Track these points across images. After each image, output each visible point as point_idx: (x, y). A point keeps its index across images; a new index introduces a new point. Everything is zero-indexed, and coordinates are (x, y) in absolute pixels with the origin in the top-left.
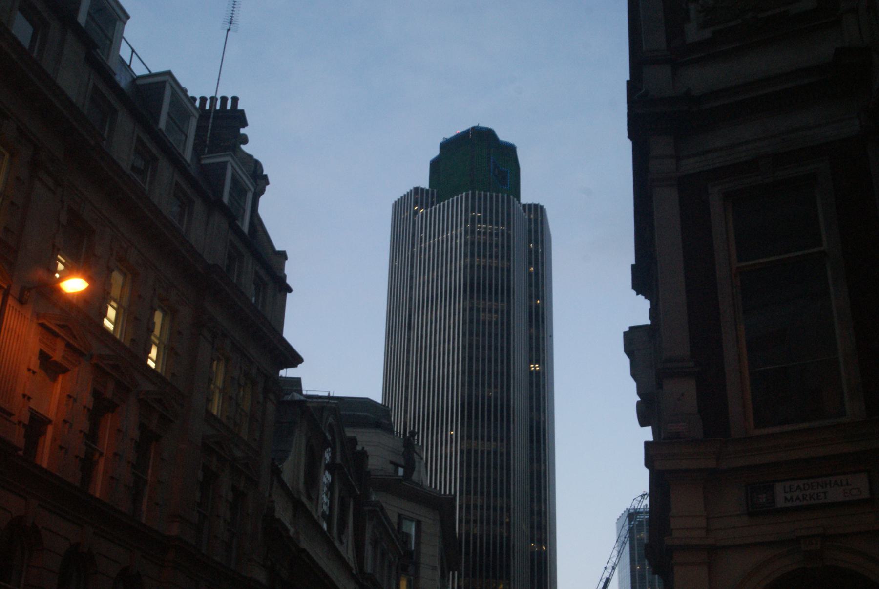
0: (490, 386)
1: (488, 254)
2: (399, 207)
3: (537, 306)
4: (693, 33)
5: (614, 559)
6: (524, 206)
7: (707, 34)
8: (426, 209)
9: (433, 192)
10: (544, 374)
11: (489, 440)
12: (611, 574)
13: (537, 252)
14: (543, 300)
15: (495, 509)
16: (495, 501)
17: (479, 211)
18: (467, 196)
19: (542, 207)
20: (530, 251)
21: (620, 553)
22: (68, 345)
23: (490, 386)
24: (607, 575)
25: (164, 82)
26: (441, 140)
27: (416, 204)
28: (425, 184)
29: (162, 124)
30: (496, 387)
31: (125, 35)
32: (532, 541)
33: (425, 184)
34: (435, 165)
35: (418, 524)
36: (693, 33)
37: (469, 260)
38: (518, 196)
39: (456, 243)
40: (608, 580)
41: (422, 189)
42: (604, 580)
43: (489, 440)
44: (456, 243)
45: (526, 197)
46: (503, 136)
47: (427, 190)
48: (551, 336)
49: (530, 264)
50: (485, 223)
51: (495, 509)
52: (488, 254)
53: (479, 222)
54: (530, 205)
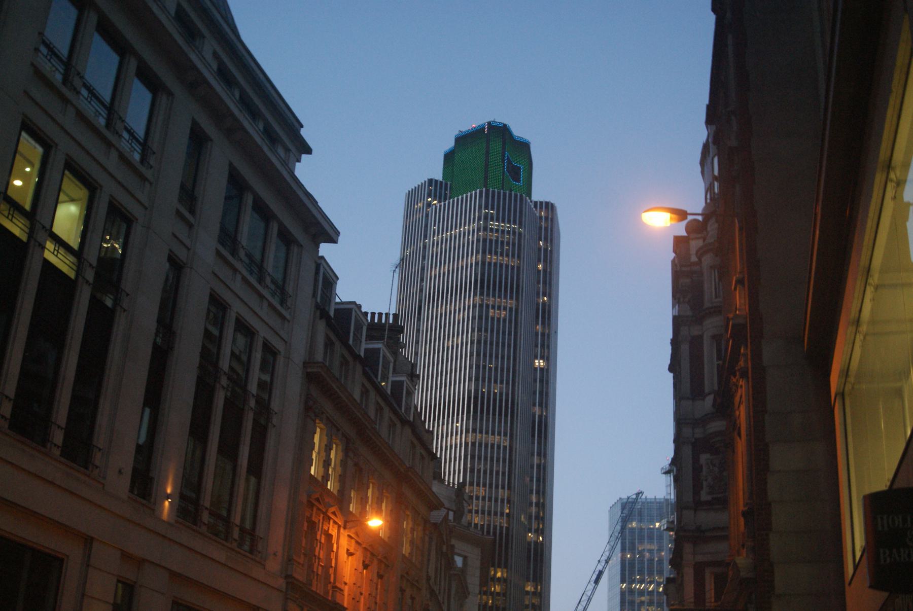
0: (496, 382)
1: (499, 250)
2: (412, 197)
3: (544, 303)
4: (705, 496)
5: (607, 554)
6: (536, 203)
7: (709, 498)
8: (440, 202)
9: (446, 184)
10: (548, 370)
11: (493, 434)
12: (604, 568)
13: (546, 250)
14: (550, 297)
15: (496, 501)
16: (497, 492)
17: (492, 209)
18: (481, 193)
19: (552, 204)
20: (540, 249)
21: (613, 549)
22: (357, 542)
23: (496, 382)
24: (600, 567)
25: (351, 310)
26: (457, 132)
27: (429, 196)
28: (438, 176)
29: (351, 342)
30: (502, 383)
31: (338, 292)
32: (530, 531)
33: (438, 176)
34: (449, 157)
35: (465, 558)
36: (705, 496)
37: (480, 256)
38: (529, 195)
39: (468, 239)
40: (601, 573)
41: (436, 181)
42: (597, 573)
43: (493, 434)
44: (468, 239)
45: (538, 194)
46: (518, 132)
47: (441, 182)
48: (556, 332)
49: (539, 261)
50: (498, 221)
51: (496, 501)
52: (499, 250)
53: (492, 220)
54: (541, 203)
